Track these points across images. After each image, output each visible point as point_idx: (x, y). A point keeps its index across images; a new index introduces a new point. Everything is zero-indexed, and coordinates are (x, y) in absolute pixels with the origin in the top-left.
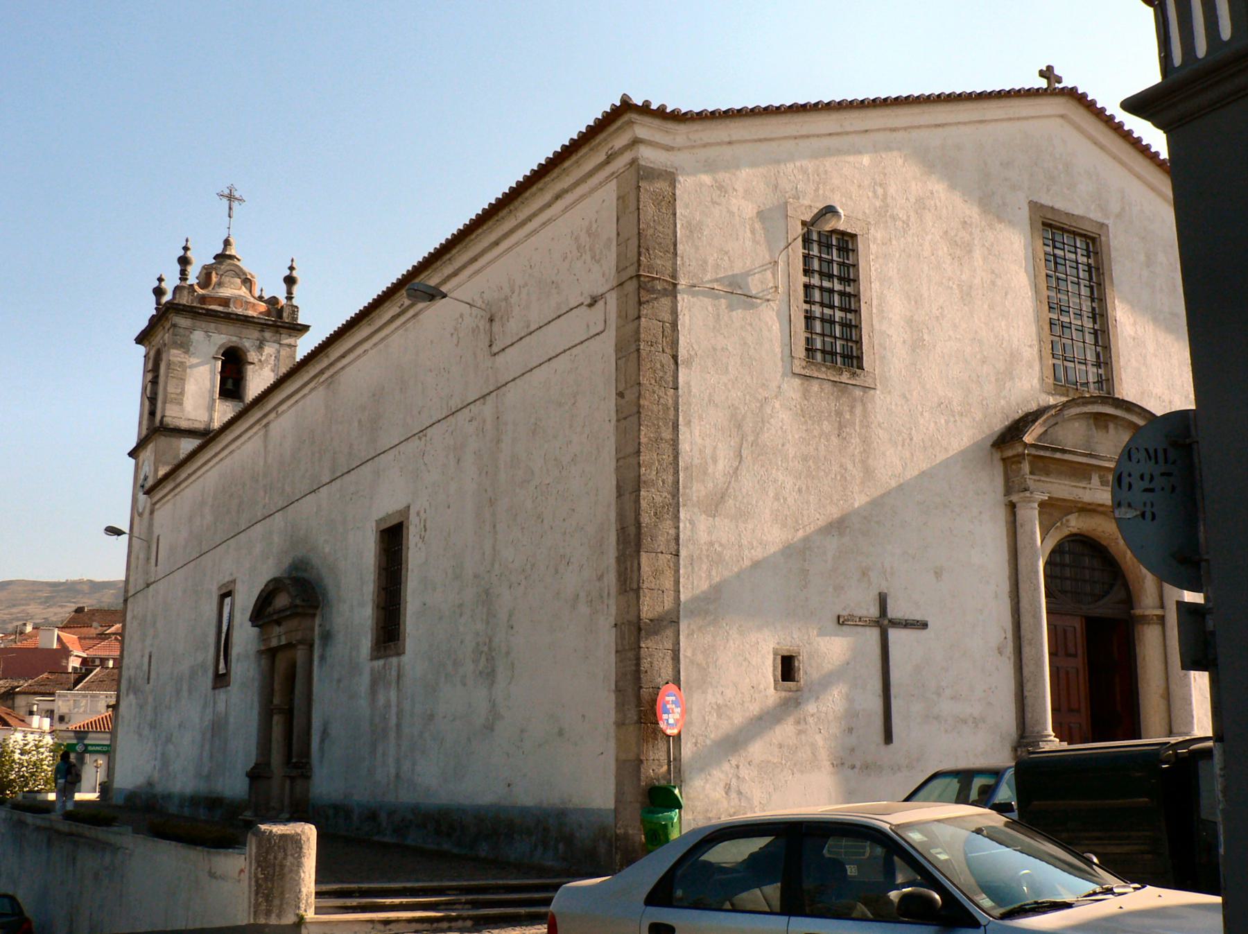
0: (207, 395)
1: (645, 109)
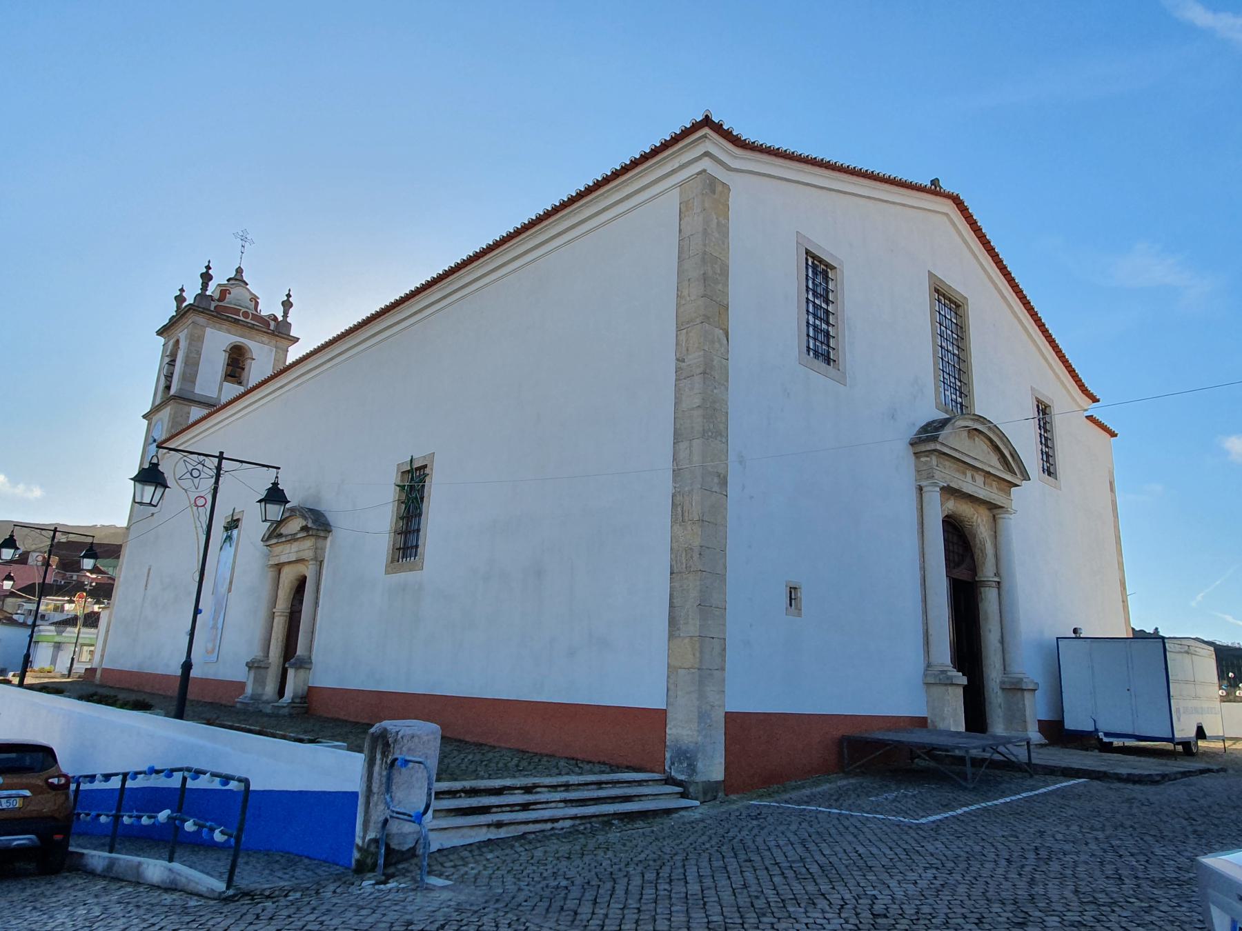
1: (718, 128)
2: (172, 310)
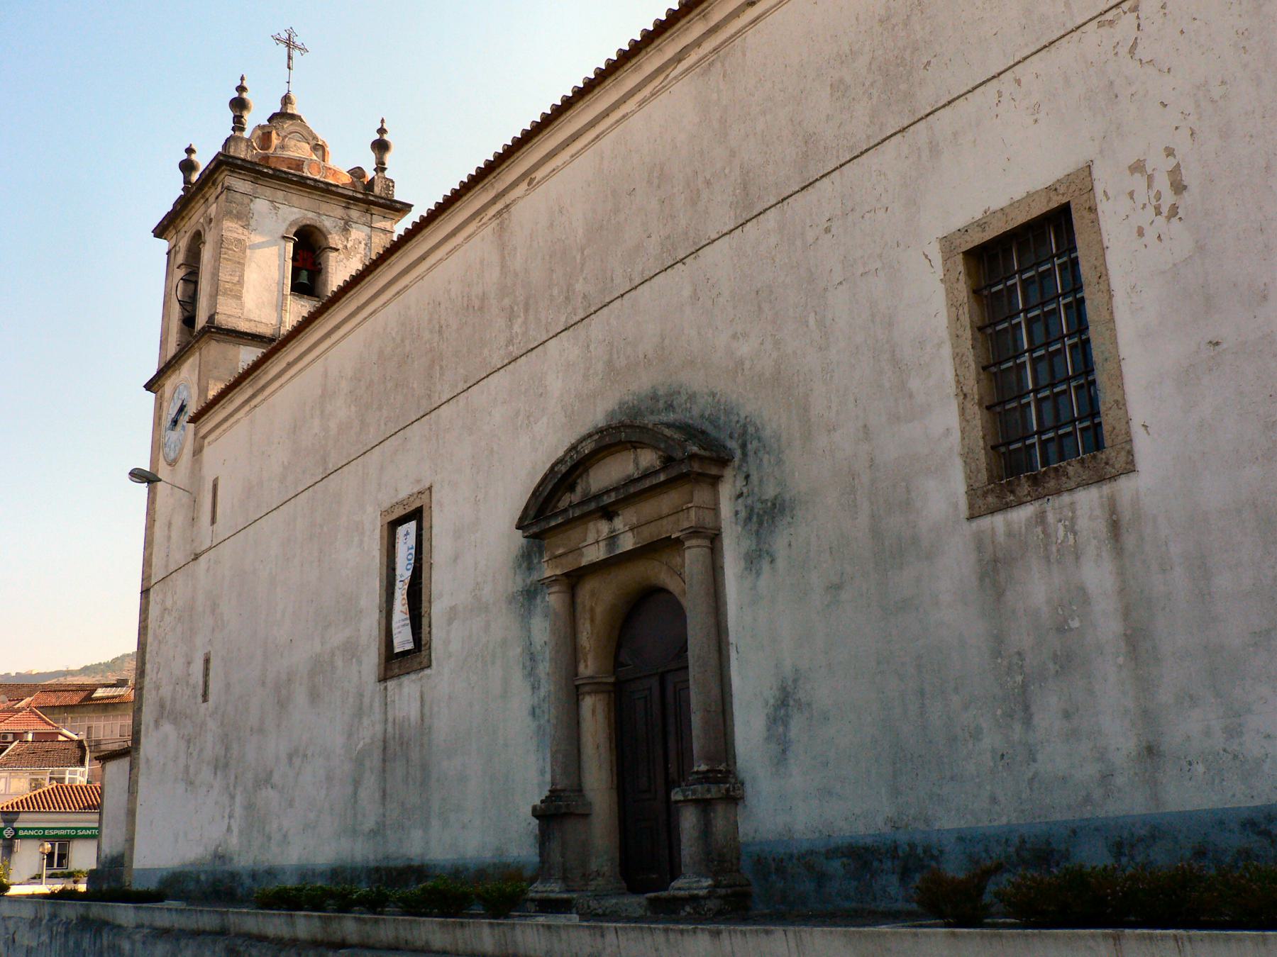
0: (274, 288)
2: (174, 188)
